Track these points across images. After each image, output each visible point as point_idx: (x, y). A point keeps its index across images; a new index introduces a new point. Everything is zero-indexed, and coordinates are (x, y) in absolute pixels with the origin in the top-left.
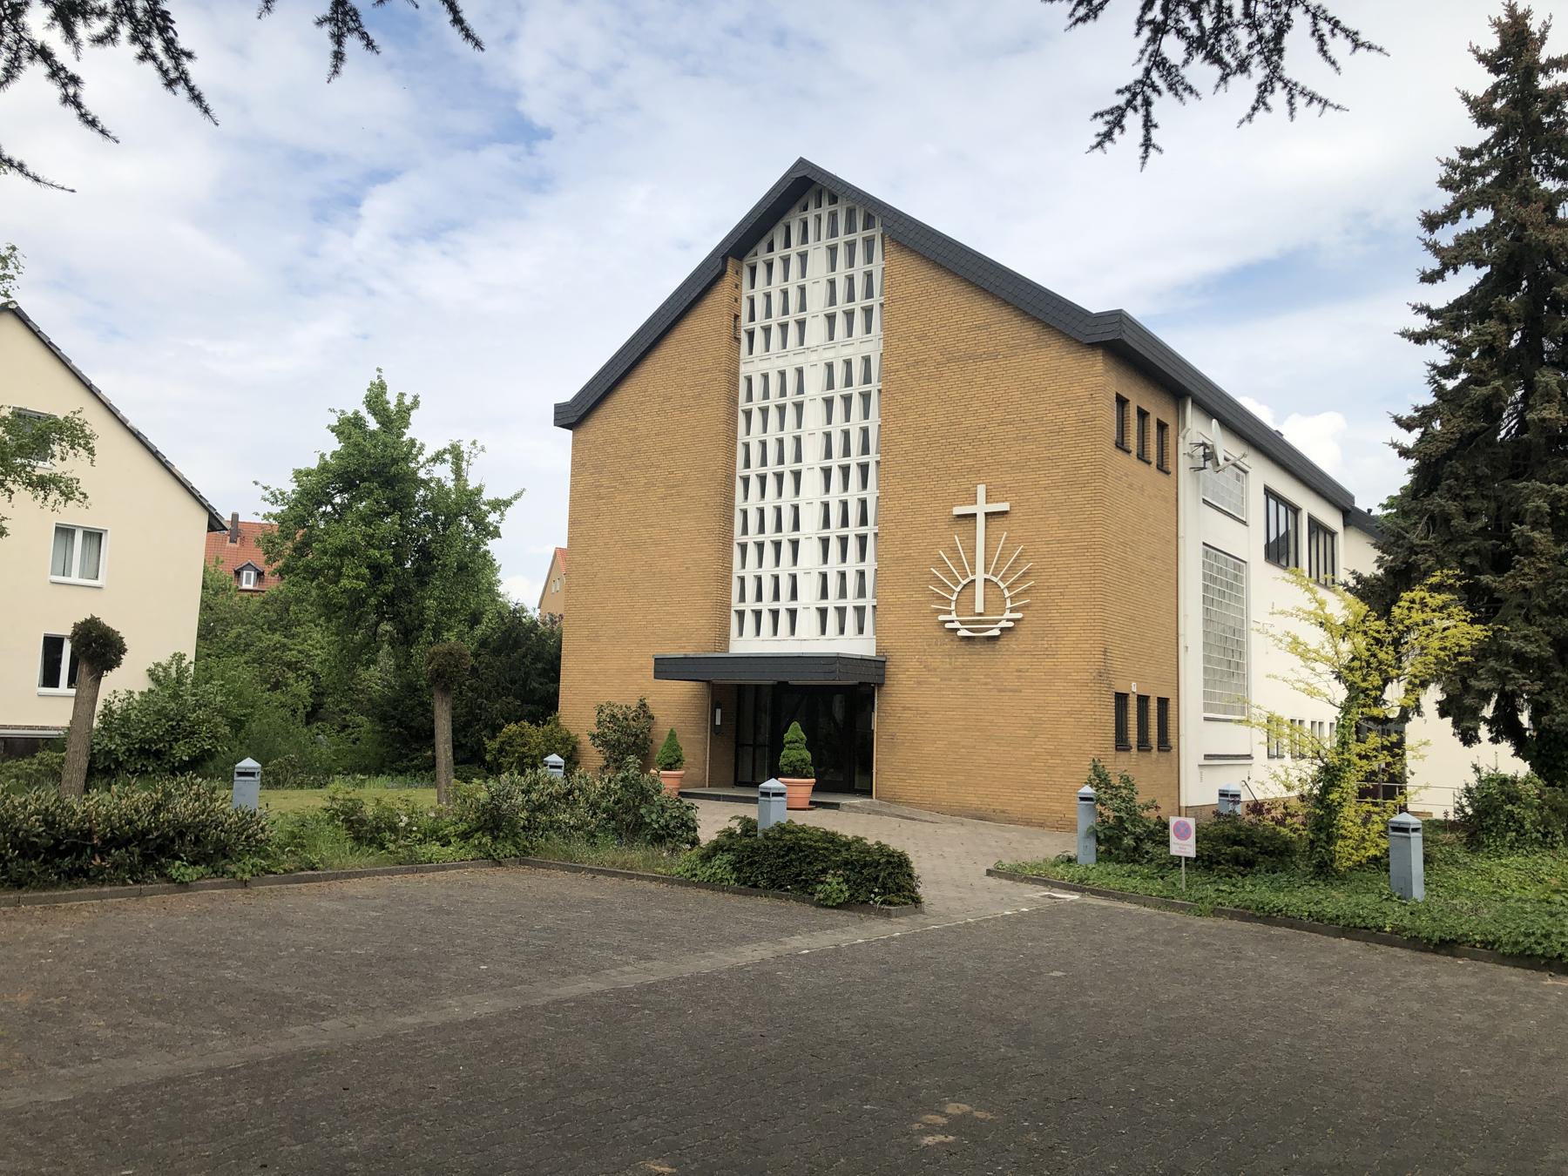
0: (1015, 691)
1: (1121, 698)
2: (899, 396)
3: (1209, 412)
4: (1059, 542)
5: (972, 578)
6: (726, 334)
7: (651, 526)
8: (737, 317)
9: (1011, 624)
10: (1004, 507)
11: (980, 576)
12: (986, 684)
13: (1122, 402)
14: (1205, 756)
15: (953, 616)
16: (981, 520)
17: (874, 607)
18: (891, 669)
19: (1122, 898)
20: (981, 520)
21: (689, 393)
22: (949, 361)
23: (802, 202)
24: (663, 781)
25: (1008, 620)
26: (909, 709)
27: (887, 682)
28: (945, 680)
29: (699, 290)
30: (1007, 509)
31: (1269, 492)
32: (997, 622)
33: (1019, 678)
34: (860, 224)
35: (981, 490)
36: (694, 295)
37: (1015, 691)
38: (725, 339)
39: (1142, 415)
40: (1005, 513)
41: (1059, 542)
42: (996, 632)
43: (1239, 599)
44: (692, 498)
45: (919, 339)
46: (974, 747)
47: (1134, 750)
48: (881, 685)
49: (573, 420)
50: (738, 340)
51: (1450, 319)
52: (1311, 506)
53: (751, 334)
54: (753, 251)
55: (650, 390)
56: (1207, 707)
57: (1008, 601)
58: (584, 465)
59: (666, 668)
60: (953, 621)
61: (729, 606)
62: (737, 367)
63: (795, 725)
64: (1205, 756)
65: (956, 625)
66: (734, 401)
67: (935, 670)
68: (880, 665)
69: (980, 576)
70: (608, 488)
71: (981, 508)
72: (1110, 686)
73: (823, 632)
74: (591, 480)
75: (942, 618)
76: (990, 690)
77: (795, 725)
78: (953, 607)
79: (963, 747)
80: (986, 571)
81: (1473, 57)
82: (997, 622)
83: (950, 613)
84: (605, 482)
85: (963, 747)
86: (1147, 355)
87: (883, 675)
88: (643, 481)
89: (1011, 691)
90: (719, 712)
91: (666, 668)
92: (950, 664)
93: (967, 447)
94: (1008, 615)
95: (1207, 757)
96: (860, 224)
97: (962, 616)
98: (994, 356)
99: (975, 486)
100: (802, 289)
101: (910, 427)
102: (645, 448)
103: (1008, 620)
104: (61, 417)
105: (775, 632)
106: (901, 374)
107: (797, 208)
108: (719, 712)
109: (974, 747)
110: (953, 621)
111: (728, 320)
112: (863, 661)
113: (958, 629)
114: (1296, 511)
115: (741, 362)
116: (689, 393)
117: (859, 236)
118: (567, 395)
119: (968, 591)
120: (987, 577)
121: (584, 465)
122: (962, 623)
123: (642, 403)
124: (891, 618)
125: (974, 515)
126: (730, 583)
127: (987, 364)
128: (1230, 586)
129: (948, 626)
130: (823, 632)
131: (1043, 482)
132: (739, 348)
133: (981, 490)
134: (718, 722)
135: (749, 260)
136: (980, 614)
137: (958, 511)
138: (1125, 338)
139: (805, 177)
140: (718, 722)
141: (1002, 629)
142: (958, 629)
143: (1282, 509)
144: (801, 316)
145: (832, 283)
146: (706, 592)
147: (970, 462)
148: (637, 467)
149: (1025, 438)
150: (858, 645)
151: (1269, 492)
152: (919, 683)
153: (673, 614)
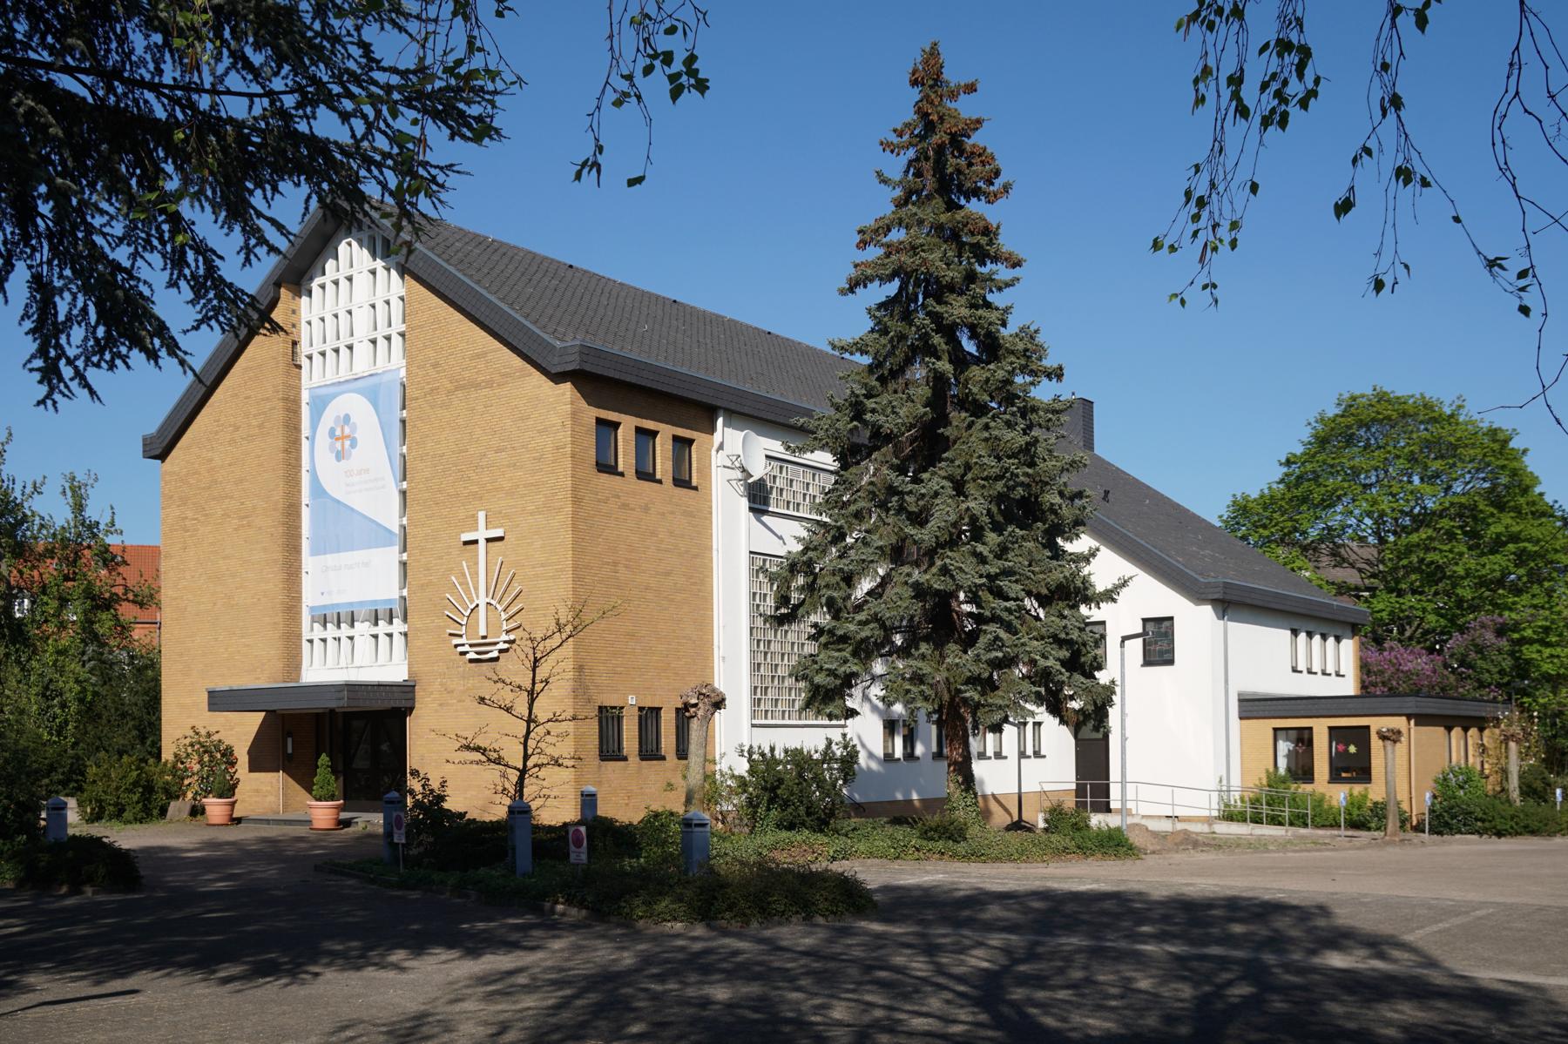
5: (476, 602)
9: (506, 646)
10: (498, 533)
16: (482, 543)
17: (406, 635)
19: (1302, 851)
20: (482, 543)
21: (254, 422)
22: (457, 388)
24: (314, 811)
27: (417, 705)
30: (502, 535)
35: (481, 515)
40: (501, 539)
42: (495, 654)
45: (435, 365)
47: (634, 759)
48: (411, 709)
49: (158, 452)
50: (299, 367)
51: (32, 331)
54: (306, 277)
56: (754, 715)
58: (171, 497)
61: (299, 636)
65: (466, 648)
69: (482, 600)
71: (481, 534)
81: (903, 105)
83: (461, 636)
84: (190, 514)
87: (413, 699)
88: (220, 512)
90: (290, 741)
94: (506, 638)
98: (490, 384)
101: (427, 454)
104: (1529, 470)
108: (290, 741)
118: (152, 428)
121: (171, 497)
122: (471, 646)
125: (475, 542)
126: (299, 613)
132: (300, 374)
133: (481, 515)
134: (290, 751)
136: (484, 637)
140: (290, 751)
141: (501, 651)
147: (475, 489)
150: (396, 672)
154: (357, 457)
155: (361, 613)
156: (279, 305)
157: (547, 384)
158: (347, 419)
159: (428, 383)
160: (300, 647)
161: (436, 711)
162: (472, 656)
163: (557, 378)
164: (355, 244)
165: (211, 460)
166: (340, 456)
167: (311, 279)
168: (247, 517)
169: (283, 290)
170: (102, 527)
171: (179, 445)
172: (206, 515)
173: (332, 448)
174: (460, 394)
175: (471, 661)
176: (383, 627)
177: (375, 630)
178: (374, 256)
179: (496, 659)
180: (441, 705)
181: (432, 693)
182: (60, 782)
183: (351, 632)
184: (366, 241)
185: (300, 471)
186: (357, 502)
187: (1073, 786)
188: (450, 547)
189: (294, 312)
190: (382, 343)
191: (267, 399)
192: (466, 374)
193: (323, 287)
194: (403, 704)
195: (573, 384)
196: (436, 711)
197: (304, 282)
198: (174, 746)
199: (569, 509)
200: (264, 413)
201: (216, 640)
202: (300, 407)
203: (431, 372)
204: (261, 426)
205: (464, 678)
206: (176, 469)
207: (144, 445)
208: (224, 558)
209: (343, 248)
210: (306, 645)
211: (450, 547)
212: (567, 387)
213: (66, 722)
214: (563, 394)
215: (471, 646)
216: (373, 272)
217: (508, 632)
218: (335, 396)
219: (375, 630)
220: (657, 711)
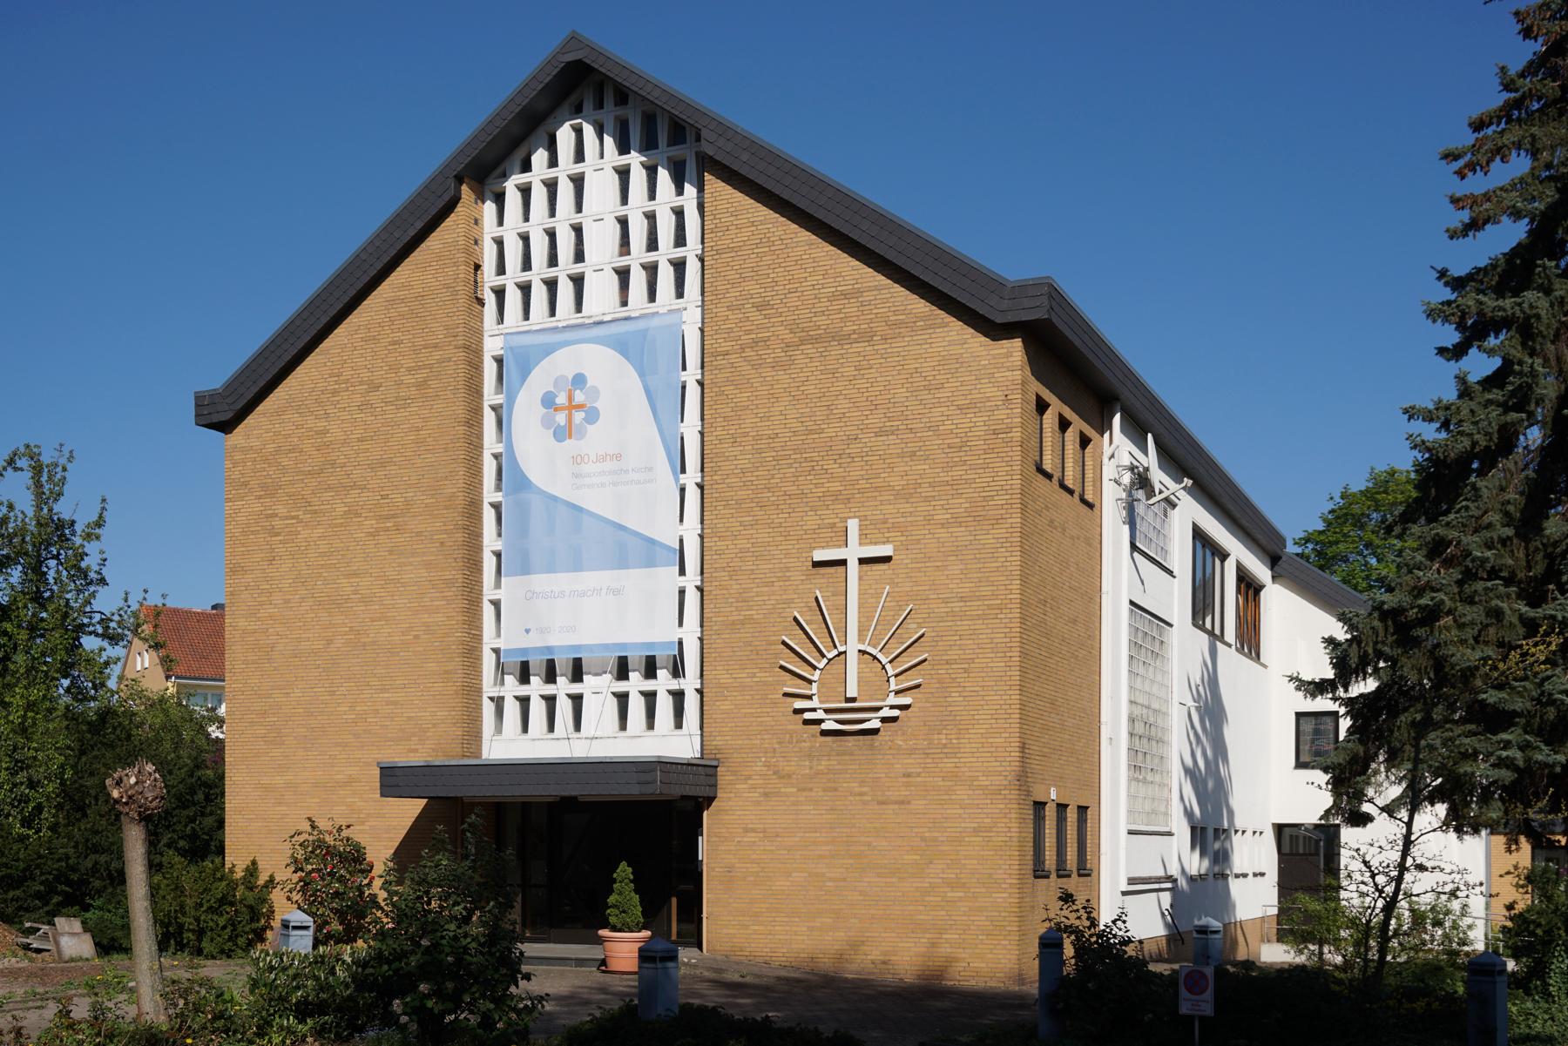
0: (902, 802)
1: (1039, 806)
2: (729, 389)
3: (1137, 430)
4: (962, 599)
5: (842, 649)
6: (463, 292)
7: (355, 574)
8: (477, 267)
9: (896, 713)
11: (853, 647)
12: (862, 794)
13: (1042, 406)
14: (1129, 879)
15: (815, 703)
16: (853, 566)
18: (724, 776)
20: (853, 566)
23: (573, 98)
25: (892, 707)
26: (754, 830)
28: (804, 790)
29: (419, 225)
31: (1199, 535)
32: (878, 709)
33: (908, 785)
34: (662, 138)
35: (853, 525)
36: (412, 232)
37: (902, 802)
38: (463, 300)
39: (1064, 425)
40: (886, 560)
41: (962, 599)
42: (875, 724)
43: (1164, 673)
44: (419, 534)
45: (759, 308)
46: (844, 880)
48: (710, 800)
50: (481, 302)
52: (1239, 552)
53: (500, 293)
54: (499, 171)
55: (347, 373)
57: (892, 680)
59: (394, 781)
60: (814, 710)
61: (479, 691)
62: (480, 342)
63: (623, 865)
64: (1129, 879)
65: (820, 715)
66: (475, 391)
67: (789, 776)
68: (710, 771)
70: (287, 518)
71: (853, 552)
72: (1028, 793)
73: (623, 727)
74: (257, 507)
75: (799, 704)
76: (865, 803)
77: (623, 865)
78: (814, 691)
79: (831, 879)
80: (861, 639)
82: (878, 709)
83: (809, 697)
84: (282, 510)
85: (831, 879)
86: (1077, 342)
87: (715, 786)
88: (341, 509)
89: (896, 803)
91: (394, 781)
92: (811, 768)
93: (830, 465)
94: (893, 700)
95: (1132, 881)
96: (662, 138)
97: (827, 702)
98: (868, 337)
99: (845, 520)
100: (578, 230)
101: (746, 435)
102: (342, 460)
103: (892, 707)
105: (551, 728)
106: (733, 358)
107: (566, 108)
109: (844, 880)
110: (814, 710)
111: (465, 271)
112: (688, 765)
113: (822, 721)
114: (1224, 556)
115: (486, 335)
116: (408, 379)
117: (635, 159)
118: (216, 379)
119: (837, 667)
120: (862, 647)
121: (245, 484)
122: (827, 711)
123: (335, 392)
124: (727, 706)
125: (843, 563)
126: (479, 659)
127: (858, 347)
128: (1155, 655)
129: (808, 716)
130: (623, 727)
131: (942, 516)
132: (481, 313)
133: (853, 525)
135: (491, 185)
137: (820, 555)
138: (1055, 320)
139: (579, 62)
141: (884, 720)
142: (822, 721)
143: (1208, 553)
144: (578, 269)
145: (623, 222)
146: (446, 672)
147: (835, 486)
148: (330, 488)
149: (913, 454)
150: (681, 745)
151: (1199, 535)
152: (766, 795)
153: (395, 703)
154: (595, 439)
155: (537, 664)
156: (459, 208)
157: (975, 342)
158: (579, 380)
159: (748, 332)
160: (479, 707)
161: (758, 803)
162: (830, 725)
163: (994, 330)
164: (589, 131)
165: (325, 432)
166: (564, 433)
167: (505, 176)
168: (394, 516)
169: (464, 188)
170: (79, 528)
171: (260, 408)
172: (315, 512)
173: (547, 422)
174: (809, 349)
175: (825, 733)
176: (636, 683)
177: (621, 686)
178: (623, 149)
179: (875, 732)
180: (766, 795)
181: (749, 777)
182: (37, 895)
183: (576, 688)
184: (610, 124)
185: (480, 454)
186: (597, 501)
187: (1275, 911)
188: (788, 569)
189: (476, 222)
190: (638, 280)
191: (436, 346)
192: (822, 321)
193: (526, 191)
194: (711, 795)
195: (1023, 342)
196: (758, 803)
197: (490, 181)
198: (288, 845)
199: (1016, 520)
200: (430, 366)
201: (332, 693)
202: (482, 362)
203: (755, 315)
204: (421, 385)
205: (810, 757)
206: (256, 443)
207: (197, 406)
208: (348, 576)
209: (565, 136)
210: (488, 709)
211: (788, 569)
212: (1014, 349)
213: (39, 808)
214: (1009, 355)
215: (827, 711)
216: (624, 173)
217: (897, 693)
218: (548, 350)
219: (621, 686)
220: (1066, 806)
